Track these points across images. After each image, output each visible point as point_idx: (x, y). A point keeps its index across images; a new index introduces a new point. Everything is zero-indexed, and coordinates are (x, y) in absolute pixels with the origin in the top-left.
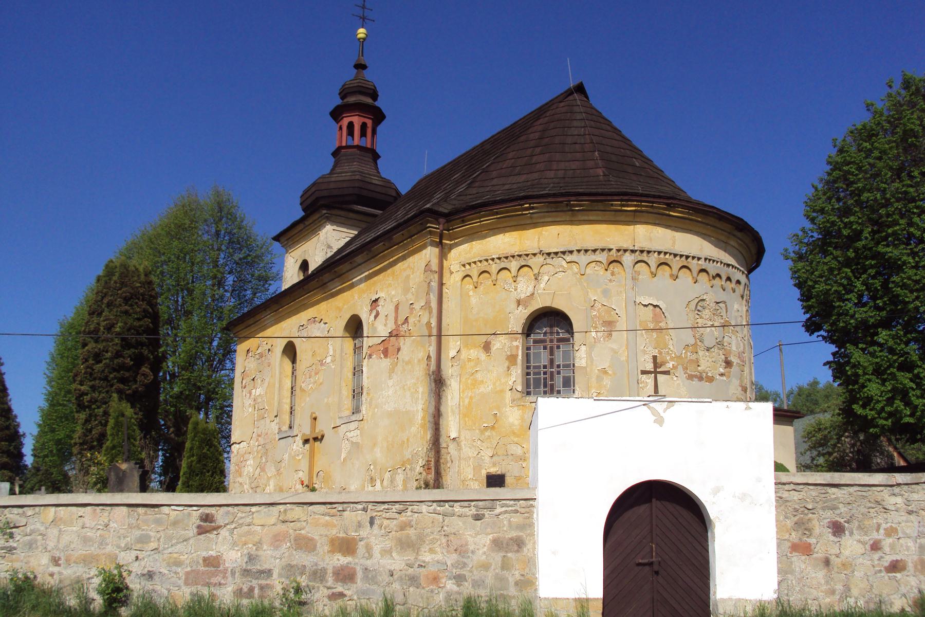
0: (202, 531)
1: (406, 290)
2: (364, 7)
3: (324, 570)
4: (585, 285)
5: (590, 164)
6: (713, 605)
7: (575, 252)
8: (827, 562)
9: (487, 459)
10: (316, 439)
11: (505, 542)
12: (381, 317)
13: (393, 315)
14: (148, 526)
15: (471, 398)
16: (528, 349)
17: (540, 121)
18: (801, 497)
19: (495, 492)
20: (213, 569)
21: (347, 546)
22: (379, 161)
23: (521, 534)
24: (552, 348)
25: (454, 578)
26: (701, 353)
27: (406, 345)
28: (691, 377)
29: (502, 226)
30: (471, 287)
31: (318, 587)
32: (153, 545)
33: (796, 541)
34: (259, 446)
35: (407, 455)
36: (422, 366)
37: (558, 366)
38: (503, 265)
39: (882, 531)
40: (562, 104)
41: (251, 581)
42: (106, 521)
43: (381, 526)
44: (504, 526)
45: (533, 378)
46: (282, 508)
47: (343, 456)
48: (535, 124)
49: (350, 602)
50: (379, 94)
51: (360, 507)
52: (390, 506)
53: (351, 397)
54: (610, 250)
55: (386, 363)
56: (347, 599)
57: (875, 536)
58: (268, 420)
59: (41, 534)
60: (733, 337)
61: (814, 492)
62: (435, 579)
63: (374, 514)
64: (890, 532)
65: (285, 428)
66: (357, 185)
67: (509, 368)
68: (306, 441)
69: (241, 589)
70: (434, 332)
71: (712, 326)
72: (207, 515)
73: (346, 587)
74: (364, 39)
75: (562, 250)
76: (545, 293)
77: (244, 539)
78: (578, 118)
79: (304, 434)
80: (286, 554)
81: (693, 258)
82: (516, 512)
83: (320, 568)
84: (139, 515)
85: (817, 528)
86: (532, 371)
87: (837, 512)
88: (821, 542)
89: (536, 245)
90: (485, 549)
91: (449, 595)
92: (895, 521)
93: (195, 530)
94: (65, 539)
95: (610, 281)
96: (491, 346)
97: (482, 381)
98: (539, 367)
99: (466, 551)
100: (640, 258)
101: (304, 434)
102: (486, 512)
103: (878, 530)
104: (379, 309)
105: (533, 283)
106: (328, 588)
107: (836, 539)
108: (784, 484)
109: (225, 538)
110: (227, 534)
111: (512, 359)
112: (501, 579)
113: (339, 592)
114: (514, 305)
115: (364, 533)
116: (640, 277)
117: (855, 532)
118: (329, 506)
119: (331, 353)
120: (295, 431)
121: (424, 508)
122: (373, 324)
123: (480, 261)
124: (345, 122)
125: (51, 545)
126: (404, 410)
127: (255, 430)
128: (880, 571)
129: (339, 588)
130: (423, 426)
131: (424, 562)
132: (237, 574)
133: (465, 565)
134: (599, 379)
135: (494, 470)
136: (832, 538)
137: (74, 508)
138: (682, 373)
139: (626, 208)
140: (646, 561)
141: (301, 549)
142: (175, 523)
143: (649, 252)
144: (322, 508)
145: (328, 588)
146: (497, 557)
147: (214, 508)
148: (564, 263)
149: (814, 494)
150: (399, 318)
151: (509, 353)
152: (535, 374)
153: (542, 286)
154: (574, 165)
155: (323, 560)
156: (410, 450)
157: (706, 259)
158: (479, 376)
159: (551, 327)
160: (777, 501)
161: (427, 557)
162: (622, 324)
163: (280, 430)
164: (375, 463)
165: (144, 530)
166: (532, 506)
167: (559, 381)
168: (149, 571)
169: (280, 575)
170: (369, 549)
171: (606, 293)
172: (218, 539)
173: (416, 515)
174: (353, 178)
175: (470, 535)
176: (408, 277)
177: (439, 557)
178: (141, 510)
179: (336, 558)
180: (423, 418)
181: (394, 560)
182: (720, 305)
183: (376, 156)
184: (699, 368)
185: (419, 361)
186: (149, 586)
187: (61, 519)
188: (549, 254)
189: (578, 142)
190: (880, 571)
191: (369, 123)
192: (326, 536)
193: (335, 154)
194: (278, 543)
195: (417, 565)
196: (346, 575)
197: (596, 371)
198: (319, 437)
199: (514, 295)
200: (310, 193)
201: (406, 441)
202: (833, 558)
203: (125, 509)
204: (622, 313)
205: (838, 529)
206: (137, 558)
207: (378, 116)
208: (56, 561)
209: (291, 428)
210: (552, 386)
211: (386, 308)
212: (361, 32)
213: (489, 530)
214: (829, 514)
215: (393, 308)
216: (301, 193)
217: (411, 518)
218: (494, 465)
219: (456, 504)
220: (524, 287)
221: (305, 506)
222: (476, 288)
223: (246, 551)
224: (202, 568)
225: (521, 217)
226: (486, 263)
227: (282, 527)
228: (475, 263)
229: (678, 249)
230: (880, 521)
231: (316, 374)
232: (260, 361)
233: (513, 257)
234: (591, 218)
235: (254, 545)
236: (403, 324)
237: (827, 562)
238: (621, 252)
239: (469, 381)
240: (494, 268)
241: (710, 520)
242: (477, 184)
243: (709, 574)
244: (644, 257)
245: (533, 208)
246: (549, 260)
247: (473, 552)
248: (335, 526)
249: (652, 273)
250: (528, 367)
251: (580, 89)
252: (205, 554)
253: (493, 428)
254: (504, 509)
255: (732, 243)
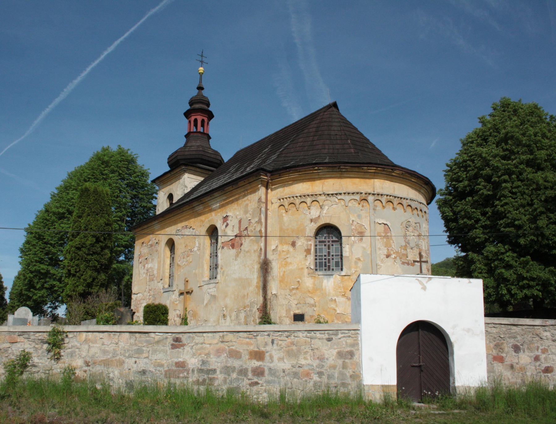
0: (174, 347)
1: (246, 212)
2: (202, 56)
3: (246, 370)
4: (348, 212)
5: (346, 146)
6: (453, 389)
7: (343, 194)
8: (512, 367)
9: (294, 306)
10: (188, 293)
11: (344, 353)
12: (230, 227)
13: (238, 225)
14: (142, 344)
15: (284, 272)
16: (316, 246)
17: (314, 122)
18: (497, 331)
19: (300, 326)
20: (181, 369)
21: (259, 355)
22: (210, 140)
23: (352, 349)
24: (329, 246)
25: (318, 373)
26: (408, 250)
27: (246, 242)
28: (403, 263)
29: (302, 178)
30: (284, 211)
31: (243, 379)
32: (145, 355)
33: (496, 355)
34: (150, 296)
35: (247, 302)
36: (256, 254)
37: (333, 256)
38: (302, 200)
39: (540, 350)
40: (326, 113)
41: (204, 376)
42: (117, 341)
43: (277, 345)
44: (343, 344)
45: (319, 262)
46: (221, 334)
47: (205, 302)
48: (312, 123)
49: (262, 388)
50: (211, 103)
51: (266, 333)
52: (282, 334)
53: (209, 270)
54: (361, 193)
55: (233, 252)
56: (260, 385)
57: (537, 353)
58: (156, 282)
59: (78, 348)
60: (423, 242)
61: (504, 328)
62: (308, 374)
63: (274, 338)
64: (544, 351)
65: (166, 286)
66: (200, 153)
67: (306, 256)
68: (182, 294)
69: (198, 380)
70: (264, 235)
71: (414, 235)
72: (177, 338)
73: (260, 379)
74: (202, 73)
75: (335, 193)
76: (326, 216)
77: (199, 352)
78: (336, 121)
79: (180, 290)
80: (224, 360)
81: (404, 199)
82: (349, 336)
83: (244, 368)
84: (136, 338)
85: (506, 348)
86: (318, 257)
87: (516, 339)
88: (508, 356)
89: (321, 189)
90: (334, 357)
91: (315, 383)
92: (547, 345)
93: (170, 347)
94: (93, 351)
95: (362, 210)
96: (296, 244)
97: (291, 263)
98: (322, 256)
99: (323, 359)
100: (377, 198)
101: (180, 290)
102: (333, 337)
103: (538, 350)
104: (228, 222)
105: (319, 210)
106: (249, 379)
107: (516, 354)
108: (489, 324)
109: (188, 351)
110: (189, 349)
111: (308, 251)
112: (342, 374)
113: (256, 382)
114: (309, 222)
115: (269, 348)
116: (377, 208)
117: (526, 351)
118: (248, 333)
119: (197, 245)
120: (174, 288)
121: (300, 334)
122: (224, 230)
123: (289, 198)
124: (193, 118)
125: (84, 354)
126: (245, 278)
127: (148, 287)
128: (540, 372)
129: (256, 380)
130: (257, 287)
131: (301, 364)
132: (196, 372)
133: (323, 366)
134: (356, 263)
135: (298, 312)
136: (514, 354)
137: (97, 334)
138: (399, 260)
139: (370, 171)
140: (417, 365)
141: (233, 357)
142: (158, 342)
143: (382, 195)
144: (245, 335)
145: (249, 379)
146: (340, 362)
147: (181, 334)
148: (336, 200)
149: (504, 329)
150: (242, 227)
151: (306, 248)
152: (320, 259)
153: (325, 212)
154: (338, 147)
155: (246, 364)
156: (249, 300)
157: (410, 199)
158: (289, 260)
159: (329, 234)
160: (485, 333)
161: (303, 362)
162: (367, 233)
163: (164, 288)
164: (226, 307)
165: (139, 346)
166: (358, 333)
167: (332, 263)
168: (143, 370)
169: (221, 373)
170: (271, 357)
171: (359, 216)
172: (184, 351)
173: (297, 338)
174: (198, 149)
175: (326, 350)
176: (247, 205)
177: (309, 362)
178: (137, 335)
179: (253, 362)
180: (258, 283)
181: (285, 363)
182: (417, 224)
183: (209, 138)
184: (408, 259)
185: (255, 251)
186: (143, 378)
187: (89, 340)
188: (328, 195)
189: (338, 134)
190: (540, 372)
191: (206, 119)
192: (247, 350)
193: (186, 136)
194: (219, 354)
195: (297, 366)
196: (259, 372)
197: (355, 259)
198: (190, 292)
199: (309, 217)
200: (174, 156)
201: (246, 294)
202: (515, 364)
203: (127, 334)
204: (367, 227)
205: (517, 349)
206: (136, 362)
207: (210, 116)
208: (87, 364)
209: (169, 286)
210: (329, 266)
211: (234, 222)
212: (201, 69)
213: (335, 347)
214: (512, 340)
215: (238, 222)
216: (168, 157)
217: (293, 340)
218: (298, 309)
219: (318, 332)
220: (315, 212)
221: (235, 333)
222: (287, 212)
223: (200, 359)
224: (174, 368)
225: (312, 174)
226: (292, 199)
227: (222, 345)
228: (286, 198)
229: (397, 194)
230: (539, 345)
231: (187, 256)
232: (150, 249)
233: (308, 195)
234: (351, 176)
235: (205, 355)
236: (244, 230)
237: (512, 367)
238: (367, 195)
239: (283, 263)
240: (297, 201)
241: (451, 343)
242: (283, 155)
243: (449, 372)
244: (380, 197)
245: (320, 169)
246: (328, 198)
247: (327, 359)
248: (252, 344)
249: (383, 206)
250: (316, 256)
251: (335, 105)
252: (176, 360)
253: (297, 288)
254: (343, 335)
255: (422, 191)
